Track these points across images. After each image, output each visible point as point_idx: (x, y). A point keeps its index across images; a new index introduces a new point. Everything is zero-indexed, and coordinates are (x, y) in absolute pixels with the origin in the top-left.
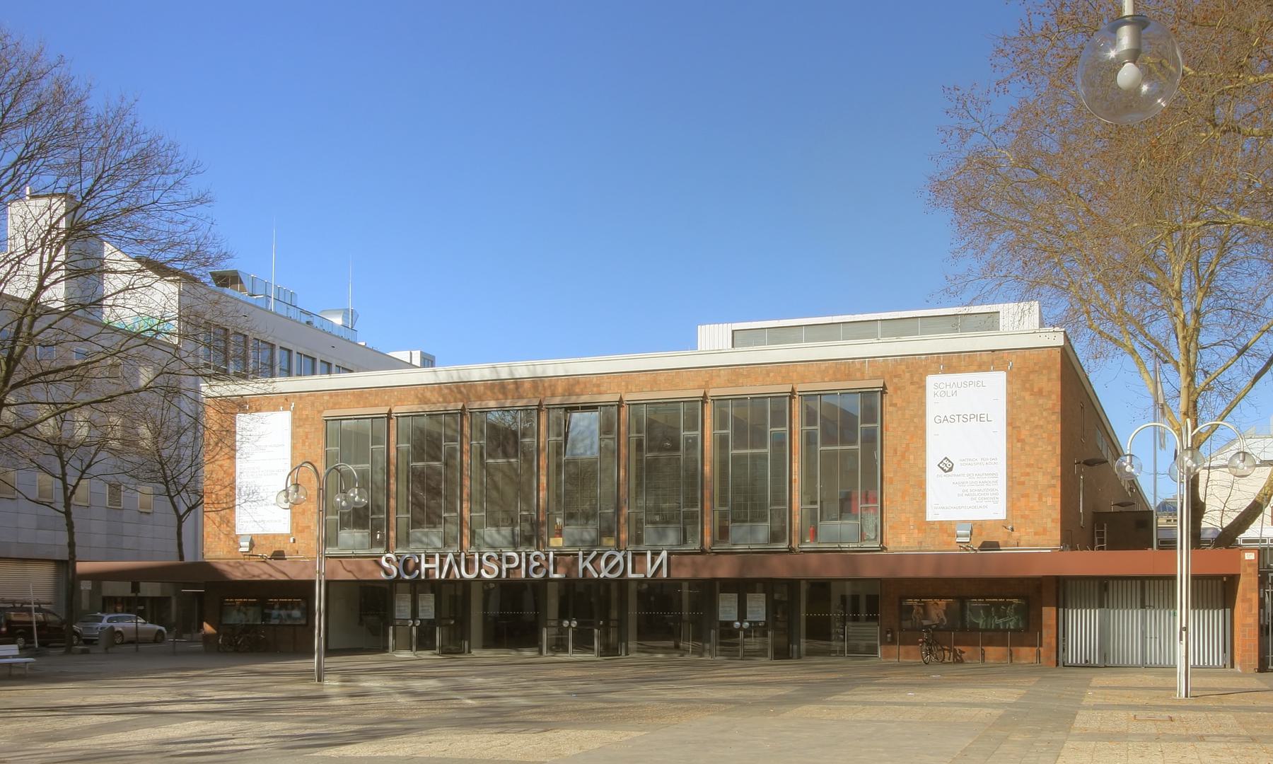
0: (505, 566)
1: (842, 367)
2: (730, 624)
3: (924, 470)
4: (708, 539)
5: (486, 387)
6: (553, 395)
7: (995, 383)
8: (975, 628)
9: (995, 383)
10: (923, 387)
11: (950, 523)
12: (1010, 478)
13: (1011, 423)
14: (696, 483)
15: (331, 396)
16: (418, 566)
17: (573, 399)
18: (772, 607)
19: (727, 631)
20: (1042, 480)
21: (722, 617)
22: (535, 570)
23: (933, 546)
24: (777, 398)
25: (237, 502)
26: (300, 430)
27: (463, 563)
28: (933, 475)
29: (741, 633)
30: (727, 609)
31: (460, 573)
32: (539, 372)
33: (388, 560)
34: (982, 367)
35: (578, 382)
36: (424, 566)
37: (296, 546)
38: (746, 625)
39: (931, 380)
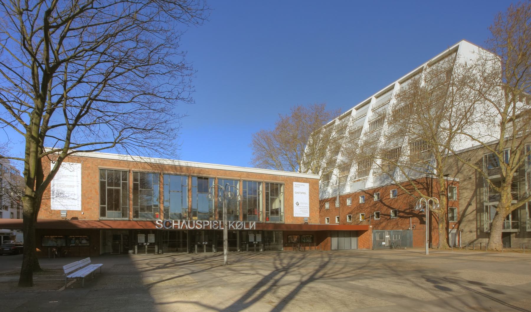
0: (204, 225)
1: (275, 177)
2: (252, 242)
3: (293, 204)
4: (131, 217)
5: (169, 167)
6: (193, 173)
7: (307, 185)
8: (303, 242)
9: (307, 185)
10: (293, 184)
11: (60, 211)
12: (310, 208)
13: (310, 195)
14: (256, 205)
15: (102, 161)
16: (171, 224)
17: (201, 175)
18: (263, 237)
19: (251, 245)
20: (316, 209)
21: (250, 241)
22: (215, 226)
23: (55, 218)
24: (125, 172)
25: (52, 197)
26: (86, 172)
27: (189, 224)
28: (295, 205)
29: (255, 245)
30: (141, 239)
31: (189, 227)
32: (189, 165)
33: (159, 222)
34: (305, 182)
35: (201, 170)
36: (174, 224)
37: (84, 216)
38: (148, 244)
39: (294, 183)
